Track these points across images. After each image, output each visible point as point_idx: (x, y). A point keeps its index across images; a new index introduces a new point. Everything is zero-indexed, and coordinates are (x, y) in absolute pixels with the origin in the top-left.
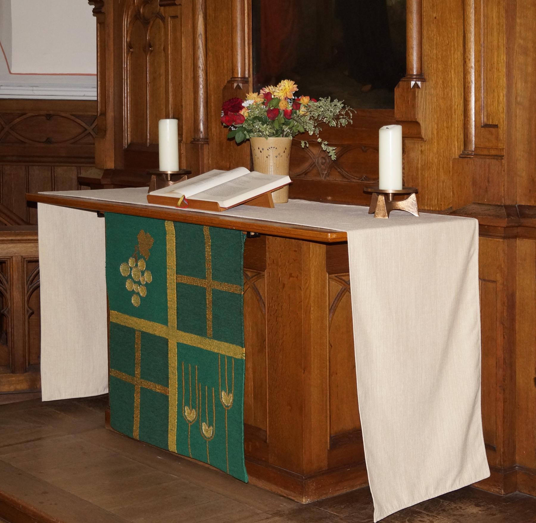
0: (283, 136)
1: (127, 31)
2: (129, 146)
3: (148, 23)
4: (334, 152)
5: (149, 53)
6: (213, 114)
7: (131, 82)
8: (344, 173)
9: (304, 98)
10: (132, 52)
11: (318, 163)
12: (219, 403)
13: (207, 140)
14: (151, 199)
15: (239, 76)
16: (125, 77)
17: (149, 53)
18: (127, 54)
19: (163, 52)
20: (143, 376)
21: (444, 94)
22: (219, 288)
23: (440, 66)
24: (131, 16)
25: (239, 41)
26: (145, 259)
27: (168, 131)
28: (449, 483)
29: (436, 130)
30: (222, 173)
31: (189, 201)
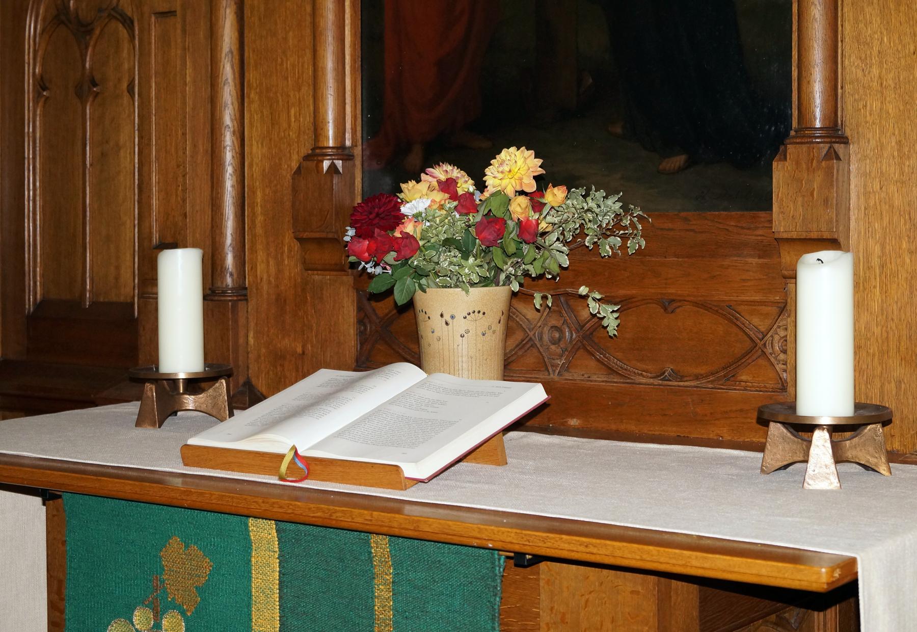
0: (497, 285)
1: (35, 52)
2: (39, 306)
3: (90, 32)
4: (616, 315)
5: (91, 99)
6: (259, 230)
7: (43, 165)
8: (614, 363)
9: (556, 190)
10: (47, 98)
11: (541, 339)
13: (242, 291)
14: (192, 455)
15: (331, 144)
16: (28, 153)
17: (91, 99)
18: (36, 103)
19: (126, 93)
21: (902, 173)
23: (890, 108)
24: (44, 19)
25: (329, 63)
26: (183, 613)
27: (180, 277)
29: (880, 257)
30: (361, 379)
31: (310, 462)
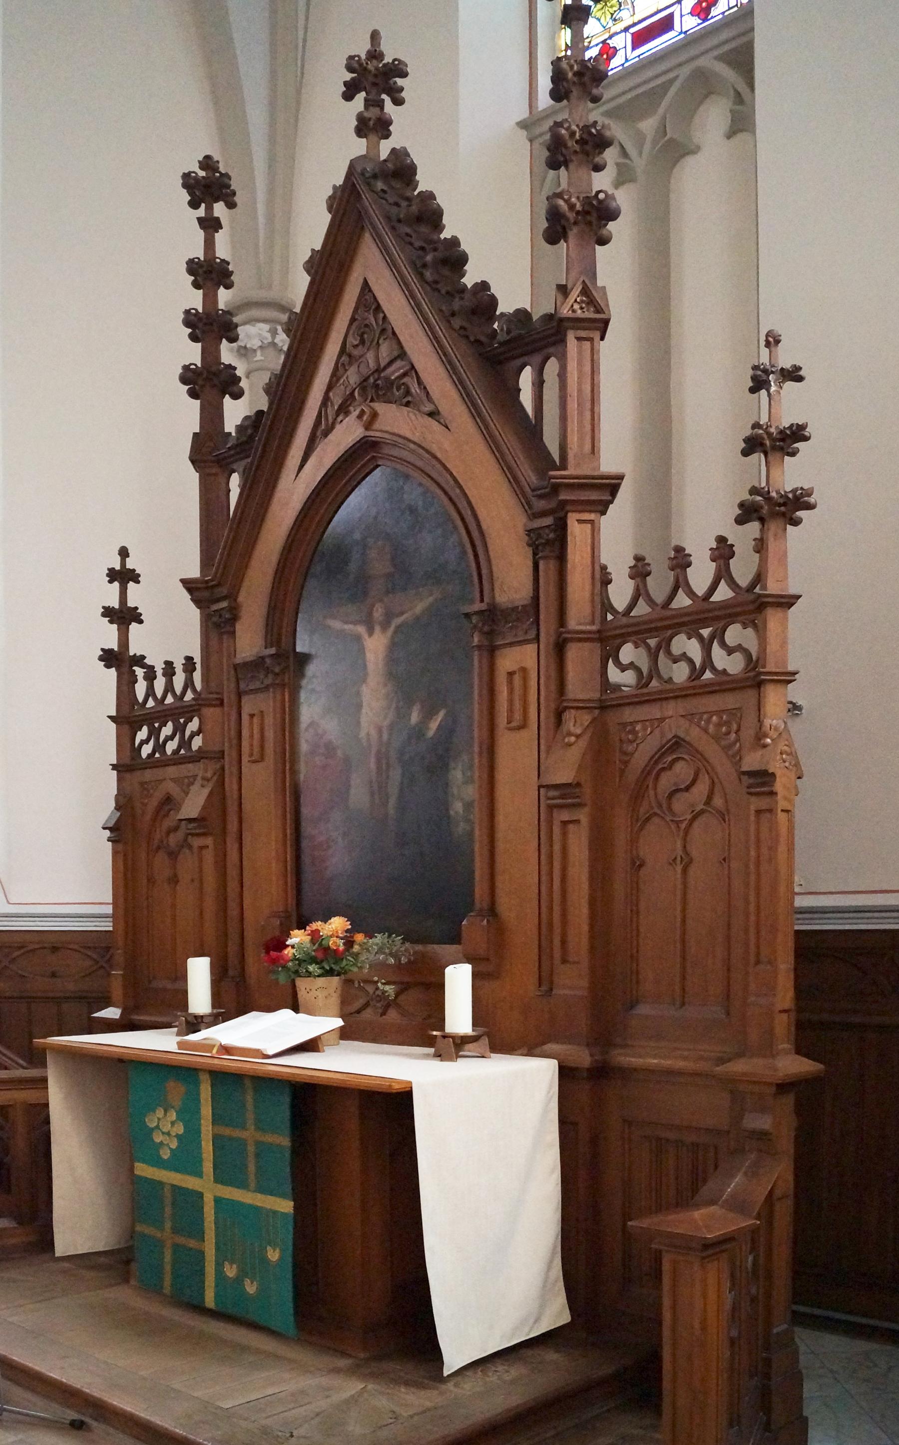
12: (264, 1260)
20: (175, 1230)
22: (262, 1139)
28: (527, 1329)
